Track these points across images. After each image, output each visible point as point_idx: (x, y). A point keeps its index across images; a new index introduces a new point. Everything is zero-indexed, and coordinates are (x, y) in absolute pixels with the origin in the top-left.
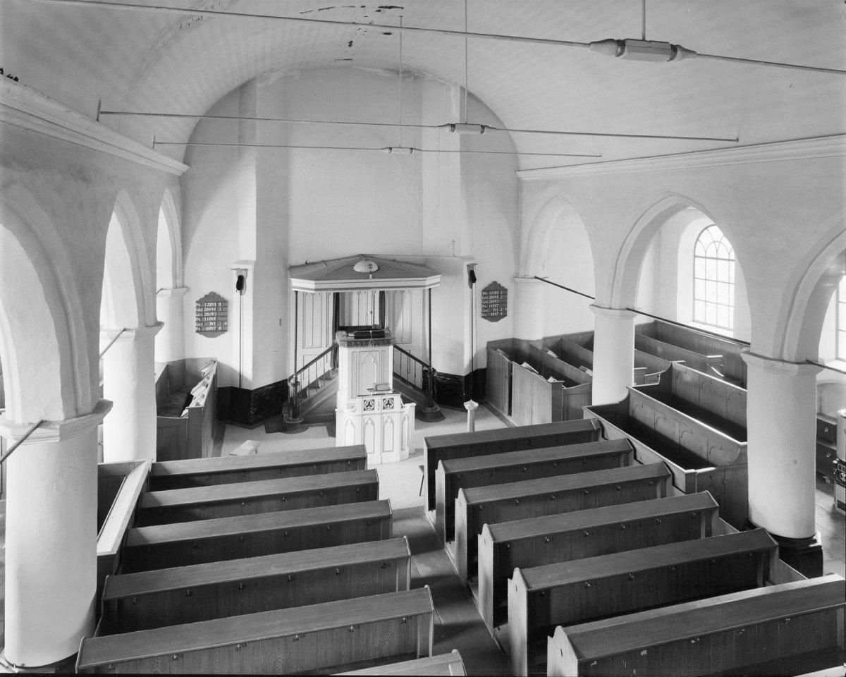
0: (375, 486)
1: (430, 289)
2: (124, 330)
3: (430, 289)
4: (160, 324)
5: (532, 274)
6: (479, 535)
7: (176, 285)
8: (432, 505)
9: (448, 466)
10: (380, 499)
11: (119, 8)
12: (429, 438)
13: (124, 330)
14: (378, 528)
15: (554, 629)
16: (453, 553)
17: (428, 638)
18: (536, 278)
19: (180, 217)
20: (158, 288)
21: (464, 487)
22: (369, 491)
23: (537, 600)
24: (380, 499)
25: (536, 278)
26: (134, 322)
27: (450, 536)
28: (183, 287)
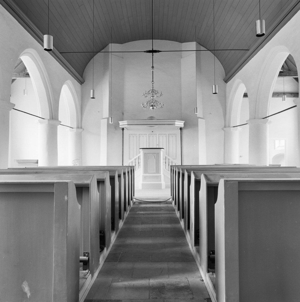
8: (171, 196)
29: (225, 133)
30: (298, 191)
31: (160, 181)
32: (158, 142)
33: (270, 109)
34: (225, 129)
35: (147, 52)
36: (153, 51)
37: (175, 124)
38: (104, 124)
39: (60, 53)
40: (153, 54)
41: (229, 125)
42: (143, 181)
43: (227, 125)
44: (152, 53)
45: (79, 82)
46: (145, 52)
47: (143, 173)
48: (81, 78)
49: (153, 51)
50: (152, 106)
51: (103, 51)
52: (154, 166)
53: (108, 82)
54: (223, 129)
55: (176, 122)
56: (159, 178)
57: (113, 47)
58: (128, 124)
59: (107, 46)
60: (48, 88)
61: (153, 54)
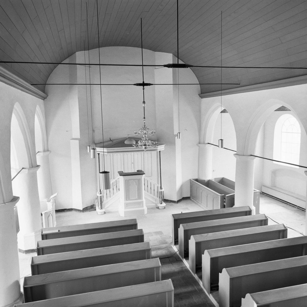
0: (142, 236)
1: (160, 151)
2: (23, 168)
3: (160, 151)
4: (38, 166)
5: (206, 142)
6: (242, 299)
7: (45, 150)
8: (176, 242)
9: (257, 299)
10: (138, 229)
11: (31, 154)
12: (174, 215)
13: (23, 168)
14: (145, 254)
15: (204, 251)
16: (187, 264)
17: (171, 298)
18: (209, 143)
19: (45, 120)
20: (37, 151)
21: (193, 235)
22: (140, 238)
23: (198, 245)
24: (138, 229)
25: (209, 143)
26: (27, 165)
27: (186, 256)
28: (48, 151)
29: (199, 148)
30: (174, 73)
31: (143, 206)
32: (132, 160)
33: (284, 194)
34: (199, 145)
35: (137, 85)
36: (144, 84)
37: (157, 150)
38: (75, 146)
39: (31, 85)
40: (144, 87)
41: (203, 142)
42: (125, 209)
43: (202, 141)
44: (142, 87)
45: (40, 98)
46: (134, 85)
47: (125, 201)
48: (44, 94)
49: (144, 84)
50: (145, 145)
51: (67, 61)
52: (136, 192)
53: (77, 98)
54: (197, 145)
55: (158, 148)
56: (141, 204)
57: (80, 56)
58: (108, 152)
59: (73, 54)
60: (25, 133)
61: (144, 87)
